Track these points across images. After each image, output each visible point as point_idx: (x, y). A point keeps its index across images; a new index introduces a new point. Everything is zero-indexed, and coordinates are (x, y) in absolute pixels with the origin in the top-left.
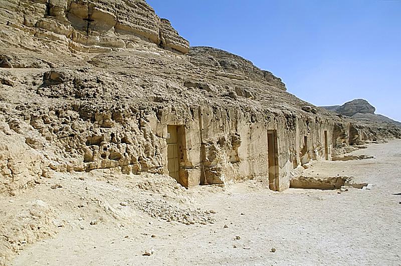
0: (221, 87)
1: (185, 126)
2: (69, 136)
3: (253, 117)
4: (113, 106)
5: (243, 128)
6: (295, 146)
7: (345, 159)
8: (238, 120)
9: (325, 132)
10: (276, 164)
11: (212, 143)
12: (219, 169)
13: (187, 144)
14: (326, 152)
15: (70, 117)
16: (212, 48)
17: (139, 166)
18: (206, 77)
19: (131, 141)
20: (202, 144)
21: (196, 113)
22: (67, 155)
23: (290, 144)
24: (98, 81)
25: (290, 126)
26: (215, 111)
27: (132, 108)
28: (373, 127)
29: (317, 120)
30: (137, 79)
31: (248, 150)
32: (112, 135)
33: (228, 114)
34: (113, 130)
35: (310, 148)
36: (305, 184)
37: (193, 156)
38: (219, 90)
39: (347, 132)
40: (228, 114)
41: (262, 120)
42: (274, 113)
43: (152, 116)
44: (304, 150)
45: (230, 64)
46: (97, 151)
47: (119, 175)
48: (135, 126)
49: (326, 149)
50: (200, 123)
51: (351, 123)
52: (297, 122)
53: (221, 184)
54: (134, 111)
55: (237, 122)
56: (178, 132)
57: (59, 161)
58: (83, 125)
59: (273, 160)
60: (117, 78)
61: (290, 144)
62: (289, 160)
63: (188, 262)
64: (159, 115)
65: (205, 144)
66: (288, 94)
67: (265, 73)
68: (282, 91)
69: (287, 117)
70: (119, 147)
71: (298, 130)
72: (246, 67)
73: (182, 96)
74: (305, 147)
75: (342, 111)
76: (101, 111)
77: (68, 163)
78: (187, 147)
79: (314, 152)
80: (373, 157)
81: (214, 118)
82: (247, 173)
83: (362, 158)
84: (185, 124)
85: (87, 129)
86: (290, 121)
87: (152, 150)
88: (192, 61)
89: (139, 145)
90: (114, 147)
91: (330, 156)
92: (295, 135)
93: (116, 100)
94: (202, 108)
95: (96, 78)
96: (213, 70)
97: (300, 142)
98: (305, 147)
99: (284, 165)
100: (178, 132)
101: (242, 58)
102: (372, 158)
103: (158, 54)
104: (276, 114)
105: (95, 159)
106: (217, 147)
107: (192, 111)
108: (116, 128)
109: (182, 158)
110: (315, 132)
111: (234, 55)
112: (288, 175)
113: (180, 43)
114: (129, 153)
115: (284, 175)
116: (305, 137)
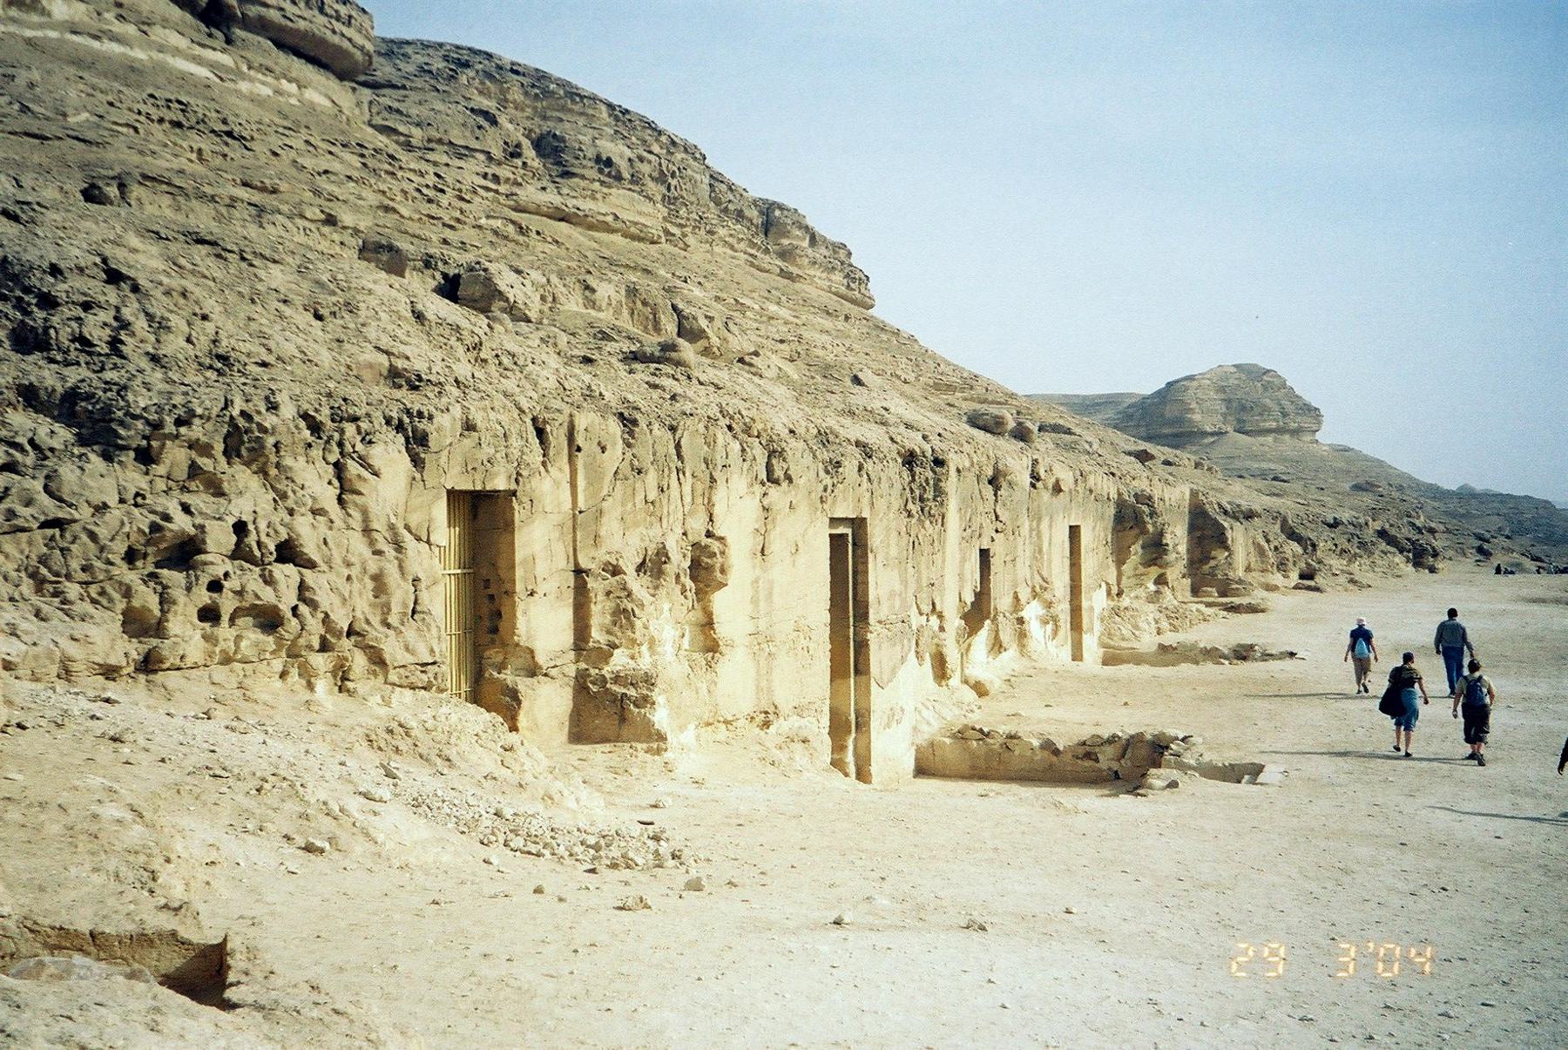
0: (554, 279)
1: (514, 493)
2: (45, 525)
3: (774, 461)
4: (228, 404)
5: (737, 508)
6: (942, 591)
7: (1167, 654)
8: (716, 475)
9: (1074, 532)
10: (862, 669)
11: (616, 571)
12: (649, 680)
13: (519, 573)
14: (1076, 625)
15: (31, 442)
16: (489, 56)
17: (351, 652)
18: (470, 221)
19: (315, 557)
20: (579, 572)
21: (557, 437)
22: (45, 609)
23: (918, 581)
24: (114, 277)
25: (922, 499)
26: (631, 433)
27: (305, 416)
28: (1301, 510)
29: (1035, 477)
30: (275, 270)
31: (755, 601)
32: (240, 528)
33: (678, 446)
34: (240, 508)
35: (1001, 600)
36: (983, 759)
37: (542, 623)
38: (543, 298)
39: (1178, 538)
40: (678, 446)
41: (812, 474)
42: (858, 444)
43: (390, 454)
44: (977, 612)
45: (591, 153)
46: (178, 593)
47: (267, 684)
48: (327, 495)
49: (1076, 611)
50: (573, 473)
51: (1194, 494)
52: (951, 484)
53: (655, 739)
54: (315, 427)
55: (713, 480)
56: (483, 516)
57: (24, 638)
58: (97, 480)
59: (850, 654)
60: (182, 261)
61: (918, 581)
62: (912, 655)
63: (1057, 489)
64: (416, 445)
65: (587, 572)
66: (882, 328)
67: (770, 221)
68: (854, 310)
69: (910, 459)
70: (269, 581)
71: (1510, 607)
72: (667, 165)
73: (485, 361)
74: (982, 596)
75: (1158, 421)
76: (179, 422)
77: (65, 643)
78: (519, 587)
79: (1021, 621)
80: (1292, 655)
81: (627, 462)
82: (746, 705)
83: (1244, 658)
84: (513, 486)
85: (122, 501)
86: (923, 470)
87: (400, 594)
88: (378, 121)
89: (346, 572)
90: (252, 580)
91: (1090, 642)
92: (942, 542)
93: (220, 373)
94: (581, 422)
95: (98, 260)
96: (496, 179)
97: (961, 576)
98: (982, 596)
99: (894, 672)
100: (483, 516)
101: (650, 125)
102: (1288, 663)
103: (203, 72)
104: (866, 450)
105: (174, 626)
106: (638, 585)
107: (540, 433)
108: (248, 495)
109: (495, 630)
110: (1025, 530)
111: (611, 106)
112: (908, 721)
113: (322, 19)
114: (313, 605)
115: (893, 717)
116: (985, 555)
